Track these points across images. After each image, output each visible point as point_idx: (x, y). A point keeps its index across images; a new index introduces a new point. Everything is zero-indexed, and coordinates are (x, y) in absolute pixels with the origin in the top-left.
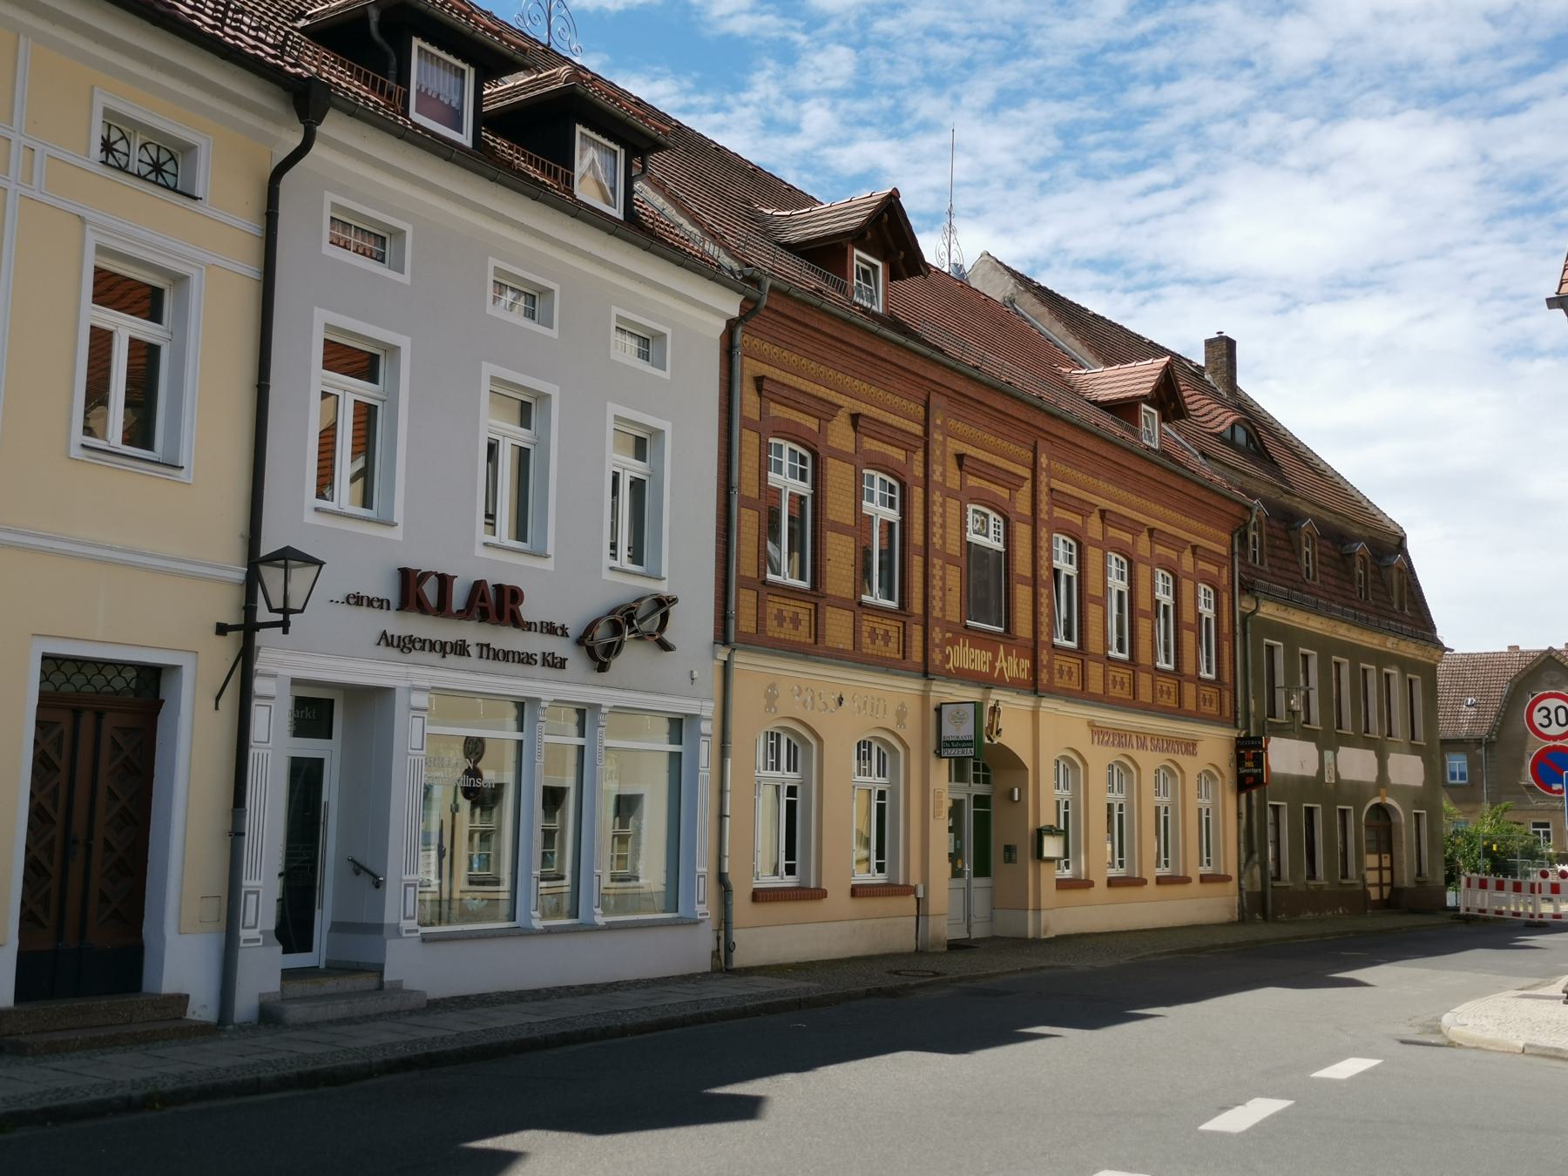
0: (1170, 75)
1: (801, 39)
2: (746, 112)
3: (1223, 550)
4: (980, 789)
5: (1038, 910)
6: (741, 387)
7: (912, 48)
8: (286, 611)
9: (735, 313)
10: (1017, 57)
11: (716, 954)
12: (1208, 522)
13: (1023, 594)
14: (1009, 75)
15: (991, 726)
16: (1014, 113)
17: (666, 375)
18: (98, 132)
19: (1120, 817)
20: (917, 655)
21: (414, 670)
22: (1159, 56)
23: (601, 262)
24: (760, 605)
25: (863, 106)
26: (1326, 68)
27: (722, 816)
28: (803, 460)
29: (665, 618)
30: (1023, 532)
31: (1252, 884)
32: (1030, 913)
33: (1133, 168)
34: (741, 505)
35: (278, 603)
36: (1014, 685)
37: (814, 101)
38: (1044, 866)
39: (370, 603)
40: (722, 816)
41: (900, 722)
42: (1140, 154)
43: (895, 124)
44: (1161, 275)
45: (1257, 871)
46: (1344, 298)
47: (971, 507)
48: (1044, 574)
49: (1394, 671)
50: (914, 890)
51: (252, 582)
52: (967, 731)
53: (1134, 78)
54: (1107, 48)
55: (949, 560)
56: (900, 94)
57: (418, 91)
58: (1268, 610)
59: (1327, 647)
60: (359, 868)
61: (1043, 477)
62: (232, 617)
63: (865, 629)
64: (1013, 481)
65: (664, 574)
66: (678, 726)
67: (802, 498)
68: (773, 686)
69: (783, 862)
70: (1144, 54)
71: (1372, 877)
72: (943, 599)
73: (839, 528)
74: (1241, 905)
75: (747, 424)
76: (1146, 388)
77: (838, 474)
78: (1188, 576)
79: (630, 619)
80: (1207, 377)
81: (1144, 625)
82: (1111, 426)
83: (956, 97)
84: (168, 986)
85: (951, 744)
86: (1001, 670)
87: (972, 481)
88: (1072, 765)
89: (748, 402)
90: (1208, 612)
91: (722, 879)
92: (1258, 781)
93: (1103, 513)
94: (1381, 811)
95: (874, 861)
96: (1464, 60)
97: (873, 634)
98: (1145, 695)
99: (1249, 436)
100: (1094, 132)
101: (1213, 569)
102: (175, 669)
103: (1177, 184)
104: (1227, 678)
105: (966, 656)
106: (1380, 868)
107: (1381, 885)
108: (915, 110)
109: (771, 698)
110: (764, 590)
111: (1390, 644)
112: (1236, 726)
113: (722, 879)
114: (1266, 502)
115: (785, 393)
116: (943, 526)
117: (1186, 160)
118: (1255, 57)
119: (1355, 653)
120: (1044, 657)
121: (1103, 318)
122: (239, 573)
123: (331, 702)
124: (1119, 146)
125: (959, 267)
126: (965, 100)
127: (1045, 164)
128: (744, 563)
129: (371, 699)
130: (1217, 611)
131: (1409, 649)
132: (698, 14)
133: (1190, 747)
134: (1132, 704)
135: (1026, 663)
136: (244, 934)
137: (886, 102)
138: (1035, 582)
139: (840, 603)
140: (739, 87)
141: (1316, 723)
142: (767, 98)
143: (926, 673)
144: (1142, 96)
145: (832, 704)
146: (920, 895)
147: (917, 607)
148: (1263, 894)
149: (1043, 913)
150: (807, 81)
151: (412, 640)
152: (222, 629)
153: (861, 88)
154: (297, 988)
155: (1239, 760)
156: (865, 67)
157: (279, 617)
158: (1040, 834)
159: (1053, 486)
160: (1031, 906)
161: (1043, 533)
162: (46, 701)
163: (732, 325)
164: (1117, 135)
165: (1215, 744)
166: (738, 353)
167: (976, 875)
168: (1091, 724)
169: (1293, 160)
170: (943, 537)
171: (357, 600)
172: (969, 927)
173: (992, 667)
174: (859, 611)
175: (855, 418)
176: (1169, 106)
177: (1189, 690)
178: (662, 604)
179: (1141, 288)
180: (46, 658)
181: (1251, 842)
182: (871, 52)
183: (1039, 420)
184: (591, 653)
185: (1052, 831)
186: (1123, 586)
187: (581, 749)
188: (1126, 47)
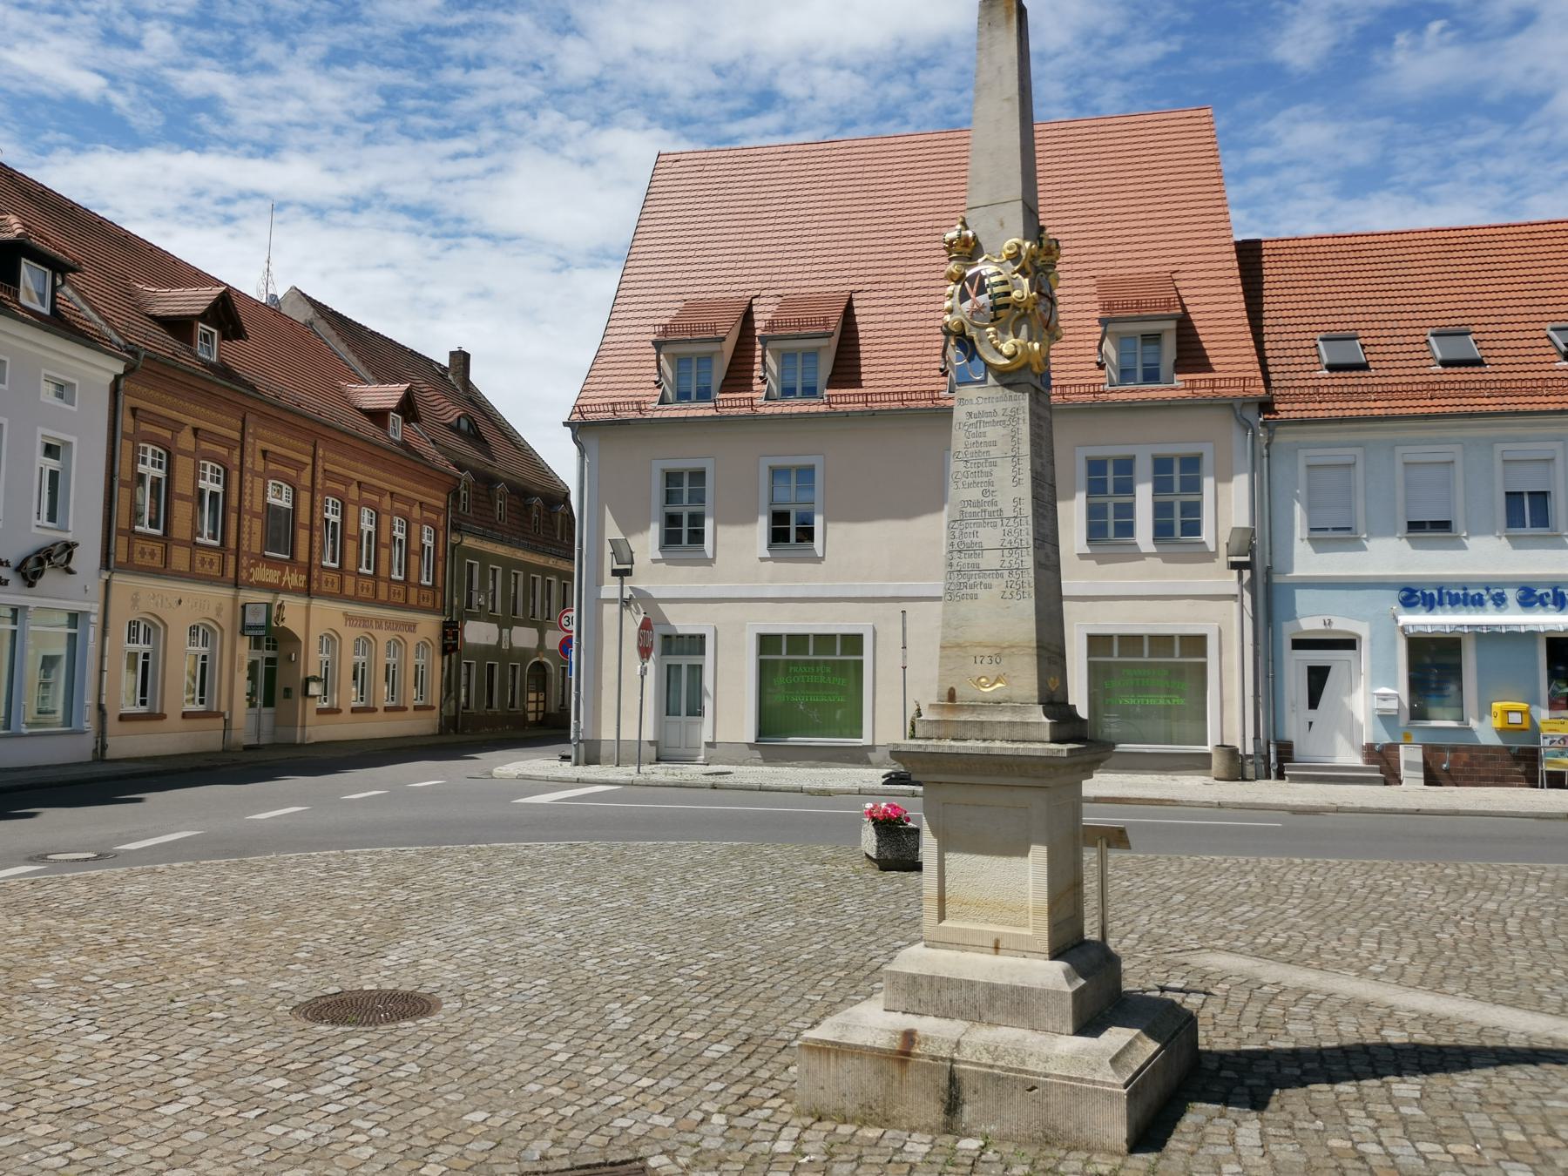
2: (85, 20)
3: (441, 505)
4: (270, 654)
5: (304, 726)
9: (121, 371)
10: (348, 21)
11: (95, 751)
12: (431, 487)
13: (303, 536)
14: (342, 36)
15: (278, 616)
16: (343, 71)
17: (74, 409)
19: (363, 671)
20: (231, 574)
22: (469, 46)
23: (38, 345)
24: (130, 545)
25: (205, 37)
26: (599, 84)
27: (101, 671)
28: (160, 456)
29: (70, 556)
30: (305, 497)
31: (449, 711)
33: (446, 134)
34: (120, 485)
36: (295, 591)
38: (309, 701)
40: (101, 671)
41: (218, 614)
42: (451, 124)
43: (234, 57)
44: (465, 227)
45: (453, 703)
46: (606, 267)
47: (270, 482)
48: (318, 522)
49: (554, 579)
50: (223, 715)
52: (261, 620)
53: (449, 59)
54: (426, 29)
55: (255, 515)
56: (241, 32)
58: (469, 542)
59: (508, 564)
61: (320, 463)
63: (198, 558)
65: (70, 528)
66: (74, 618)
67: (159, 479)
68: (136, 594)
69: (139, 698)
70: (457, 41)
71: (532, 707)
72: (250, 540)
73: (183, 497)
74: (440, 724)
75: (125, 436)
77: (183, 465)
78: (416, 521)
79: (48, 557)
80: (450, 377)
81: (384, 553)
82: (369, 429)
83: (293, 47)
85: (251, 627)
87: (272, 466)
88: (330, 640)
89: (126, 422)
90: (429, 543)
91: (100, 707)
92: (455, 648)
93: (359, 483)
94: (540, 666)
95: (198, 697)
96: (698, 97)
97: (203, 561)
98: (383, 595)
99: (469, 423)
100: (413, 98)
101: (434, 517)
103: (480, 154)
104: (439, 584)
105: (263, 574)
106: (537, 702)
107: (537, 711)
108: (254, 50)
109: (135, 601)
110: (133, 537)
111: (552, 562)
113: (100, 707)
114: (474, 472)
115: (151, 417)
116: (252, 495)
117: (489, 136)
118: (544, 64)
119: (527, 567)
120: (315, 573)
124: (434, 115)
125: (274, 297)
126: (300, 51)
127: (369, 118)
128: (122, 518)
131: (562, 565)
133: (412, 627)
134: (374, 602)
135: (303, 578)
137: (227, 37)
138: (311, 528)
139: (182, 543)
141: (499, 613)
142: (108, 10)
143: (237, 584)
144: (453, 75)
145: (175, 604)
147: (232, 544)
148: (456, 716)
155: (445, 635)
158: (307, 681)
160: (299, 724)
161: (318, 497)
163: (117, 378)
164: (432, 104)
165: (429, 626)
166: (121, 394)
167: (265, 706)
168: (345, 614)
169: (570, 151)
170: (251, 502)
173: (281, 581)
175: (196, 431)
176: (476, 88)
177: (413, 592)
178: (69, 547)
179: (447, 235)
181: (450, 685)
183: (318, 428)
184: (24, 576)
186: (372, 528)
187: (14, 632)
188: (444, 32)
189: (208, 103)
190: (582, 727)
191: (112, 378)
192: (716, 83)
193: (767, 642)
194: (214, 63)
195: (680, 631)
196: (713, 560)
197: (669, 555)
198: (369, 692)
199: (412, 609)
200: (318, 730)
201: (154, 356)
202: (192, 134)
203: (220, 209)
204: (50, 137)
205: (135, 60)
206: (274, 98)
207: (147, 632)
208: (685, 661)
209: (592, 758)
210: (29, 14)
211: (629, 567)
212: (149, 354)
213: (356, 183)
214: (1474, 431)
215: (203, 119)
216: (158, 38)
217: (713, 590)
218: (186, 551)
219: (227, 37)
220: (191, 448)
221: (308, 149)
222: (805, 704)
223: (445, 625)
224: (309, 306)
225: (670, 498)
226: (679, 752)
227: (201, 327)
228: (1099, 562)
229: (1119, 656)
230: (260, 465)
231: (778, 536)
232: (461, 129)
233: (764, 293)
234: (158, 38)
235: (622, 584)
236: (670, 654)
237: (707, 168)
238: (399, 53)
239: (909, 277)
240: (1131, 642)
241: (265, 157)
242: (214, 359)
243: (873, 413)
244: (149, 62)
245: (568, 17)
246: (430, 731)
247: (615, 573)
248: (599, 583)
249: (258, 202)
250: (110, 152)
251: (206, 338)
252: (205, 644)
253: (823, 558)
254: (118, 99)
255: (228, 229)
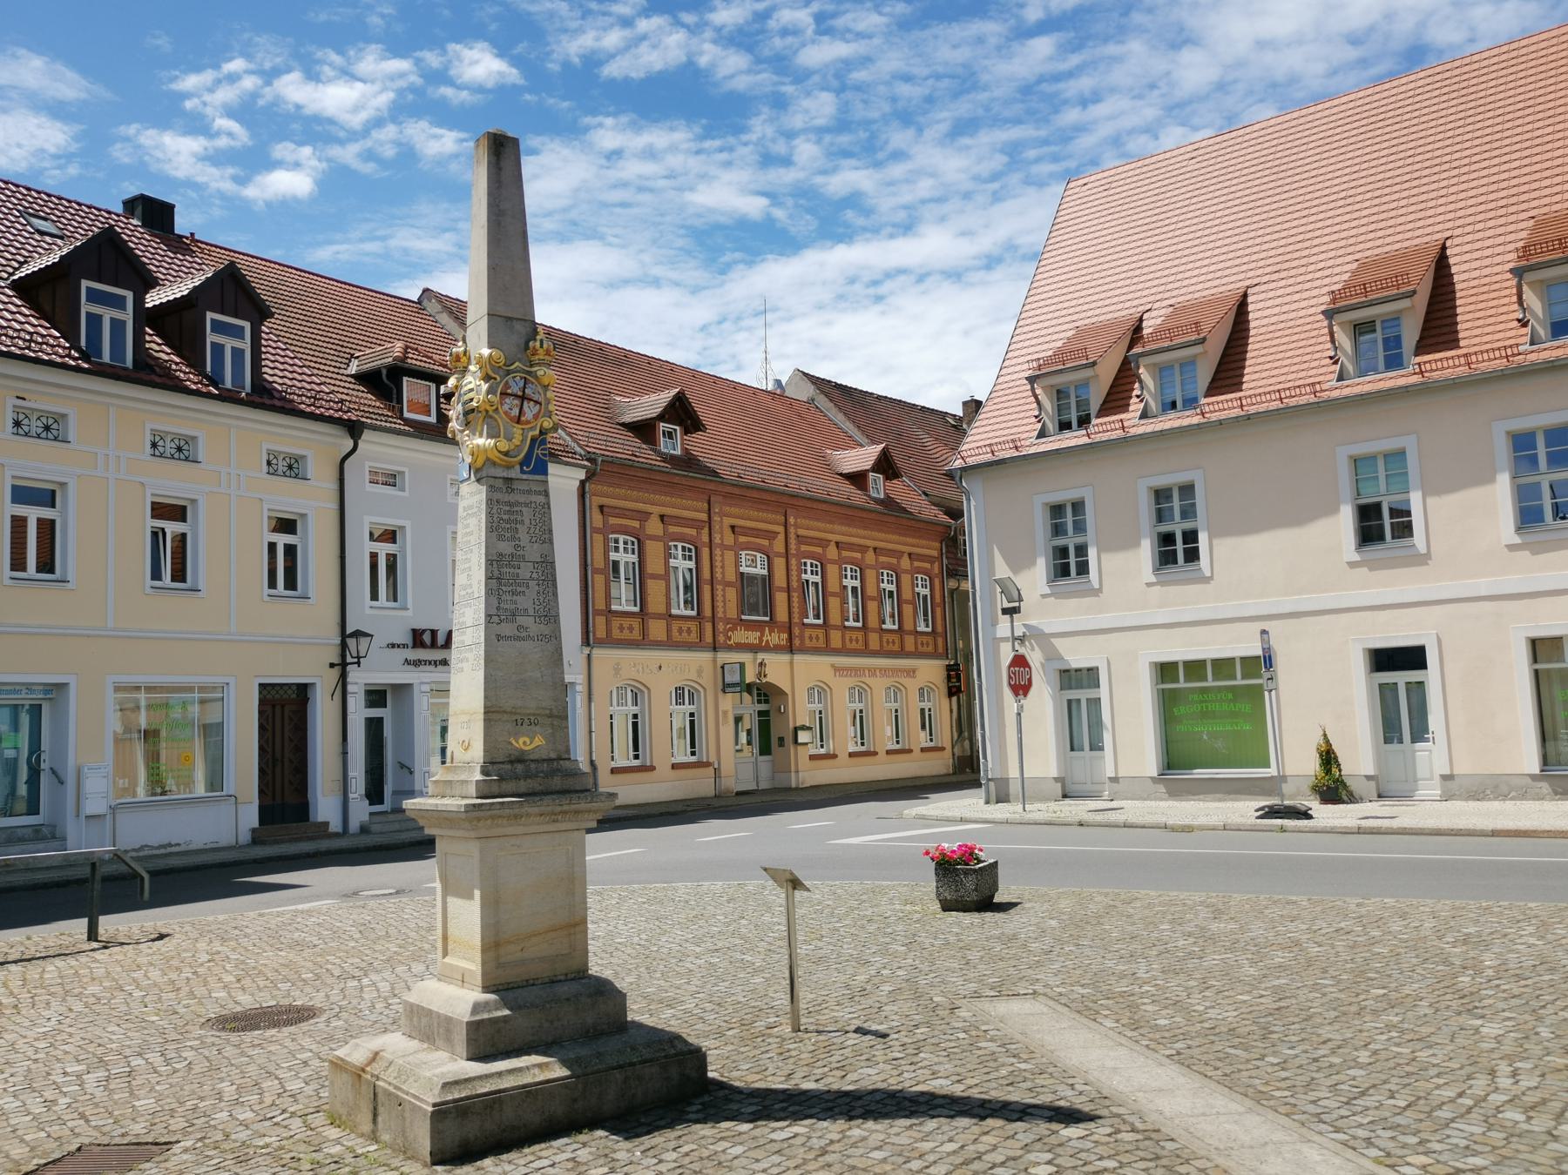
0: (1095, 98)
1: (789, 89)
3: (935, 553)
5: (797, 772)
6: (591, 512)
7: (882, 89)
8: (358, 657)
10: (968, 91)
13: (780, 599)
14: (963, 108)
16: (966, 141)
18: (265, 458)
19: (930, 715)
20: (709, 638)
21: (422, 674)
22: (1085, 83)
24: (608, 623)
25: (844, 139)
26: (1221, 87)
27: (590, 732)
30: (779, 563)
32: (793, 774)
35: (355, 654)
36: (777, 649)
37: (802, 137)
38: (799, 748)
39: (399, 646)
42: (1072, 164)
43: (871, 152)
47: (743, 553)
48: (795, 584)
51: (344, 646)
53: (1065, 102)
54: (1041, 79)
56: (875, 127)
57: (408, 401)
60: (402, 766)
61: (792, 530)
62: (336, 660)
64: (771, 536)
68: (618, 664)
75: (595, 530)
76: (868, 465)
77: (654, 549)
83: (920, 130)
84: (320, 819)
86: (767, 641)
87: (742, 539)
88: (820, 691)
89: (596, 519)
96: (1333, 73)
97: (680, 631)
100: (1034, 148)
102: (313, 684)
104: (939, 629)
105: (741, 636)
108: (886, 142)
109: (617, 670)
110: (610, 615)
112: (947, 658)
115: (617, 511)
120: (796, 631)
121: (886, 397)
122: (338, 641)
123: (385, 691)
124: (1055, 159)
127: (995, 177)
129: (403, 689)
130: (932, 590)
132: (707, 76)
133: (911, 673)
134: (866, 652)
135: (785, 636)
136: (351, 796)
137: (863, 135)
138: (788, 589)
140: (739, 130)
142: (764, 137)
143: (715, 648)
144: (1072, 116)
146: (716, 766)
147: (708, 612)
149: (800, 774)
150: (797, 121)
151: (420, 661)
152: (332, 665)
153: (842, 125)
154: (377, 819)
155: (949, 678)
156: (844, 108)
157: (356, 660)
158: (796, 729)
159: (799, 533)
160: (793, 768)
161: (793, 562)
162: (262, 702)
163: (583, 483)
164: (1053, 149)
168: (833, 666)
170: (723, 573)
171: (393, 646)
172: (757, 783)
173: (761, 639)
174: (670, 619)
180: (260, 685)
182: (848, 95)
183: (785, 499)
185: (804, 728)
188: (1057, 78)
189: (854, 200)
190: (990, 765)
191: (578, 483)
192: (1352, 53)
193: (1165, 671)
194: (853, 162)
195: (1075, 665)
196: (1100, 590)
197: (1163, 578)
198: (937, 732)
199: (908, 655)
200: (810, 775)
201: (610, 459)
202: (841, 230)
203: (871, 291)
204: (727, 258)
205: (788, 176)
206: (907, 181)
207: (691, 695)
208: (1083, 695)
209: (1002, 798)
210: (703, 157)
211: (1016, 604)
212: (605, 458)
213: (986, 243)
214: (651, 483)
215: (849, 215)
216: (806, 151)
217: (1105, 621)
218: (663, 623)
219: (863, 135)
220: (660, 533)
221: (942, 219)
222: (1209, 733)
223: (949, 668)
224: (809, 384)
225: (1161, 516)
226: (1089, 787)
227: (663, 426)
228: (1535, 553)
229: (1243, 678)
230: (729, 539)
231: (1166, 558)
232: (1084, 165)
233: (1157, 305)
234: (806, 151)
235: (1012, 622)
236: (1070, 688)
237: (1114, 185)
238: (1017, 109)
239: (1313, 259)
240: (1195, 668)
241: (905, 234)
242: (678, 452)
243: (1249, 417)
244: (801, 175)
245: (1182, 30)
246: (943, 771)
247: (1005, 611)
248: (994, 623)
249: (902, 278)
250: (776, 260)
251: (670, 435)
252: (691, 702)
253: (1211, 578)
254: (779, 213)
255: (879, 308)
